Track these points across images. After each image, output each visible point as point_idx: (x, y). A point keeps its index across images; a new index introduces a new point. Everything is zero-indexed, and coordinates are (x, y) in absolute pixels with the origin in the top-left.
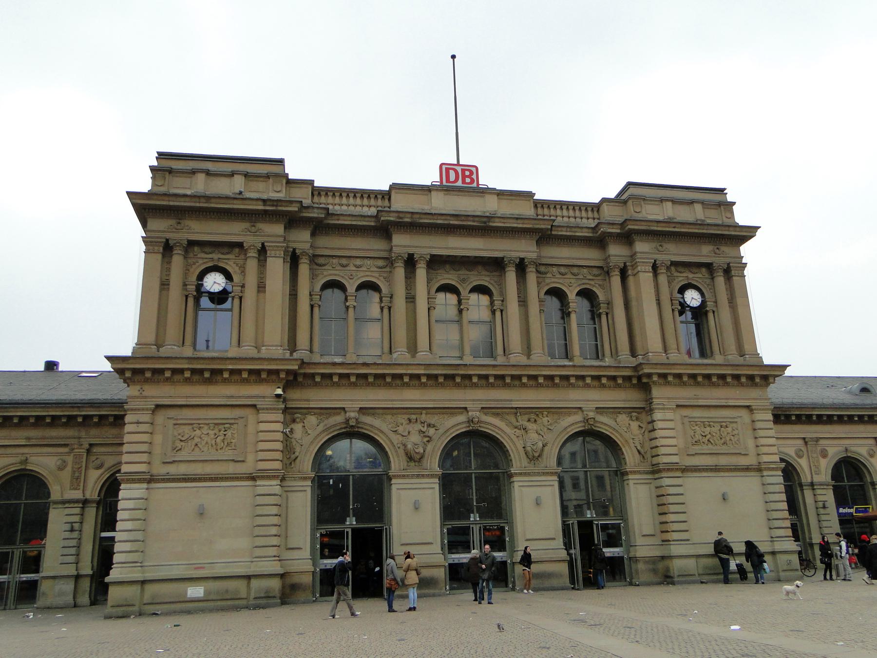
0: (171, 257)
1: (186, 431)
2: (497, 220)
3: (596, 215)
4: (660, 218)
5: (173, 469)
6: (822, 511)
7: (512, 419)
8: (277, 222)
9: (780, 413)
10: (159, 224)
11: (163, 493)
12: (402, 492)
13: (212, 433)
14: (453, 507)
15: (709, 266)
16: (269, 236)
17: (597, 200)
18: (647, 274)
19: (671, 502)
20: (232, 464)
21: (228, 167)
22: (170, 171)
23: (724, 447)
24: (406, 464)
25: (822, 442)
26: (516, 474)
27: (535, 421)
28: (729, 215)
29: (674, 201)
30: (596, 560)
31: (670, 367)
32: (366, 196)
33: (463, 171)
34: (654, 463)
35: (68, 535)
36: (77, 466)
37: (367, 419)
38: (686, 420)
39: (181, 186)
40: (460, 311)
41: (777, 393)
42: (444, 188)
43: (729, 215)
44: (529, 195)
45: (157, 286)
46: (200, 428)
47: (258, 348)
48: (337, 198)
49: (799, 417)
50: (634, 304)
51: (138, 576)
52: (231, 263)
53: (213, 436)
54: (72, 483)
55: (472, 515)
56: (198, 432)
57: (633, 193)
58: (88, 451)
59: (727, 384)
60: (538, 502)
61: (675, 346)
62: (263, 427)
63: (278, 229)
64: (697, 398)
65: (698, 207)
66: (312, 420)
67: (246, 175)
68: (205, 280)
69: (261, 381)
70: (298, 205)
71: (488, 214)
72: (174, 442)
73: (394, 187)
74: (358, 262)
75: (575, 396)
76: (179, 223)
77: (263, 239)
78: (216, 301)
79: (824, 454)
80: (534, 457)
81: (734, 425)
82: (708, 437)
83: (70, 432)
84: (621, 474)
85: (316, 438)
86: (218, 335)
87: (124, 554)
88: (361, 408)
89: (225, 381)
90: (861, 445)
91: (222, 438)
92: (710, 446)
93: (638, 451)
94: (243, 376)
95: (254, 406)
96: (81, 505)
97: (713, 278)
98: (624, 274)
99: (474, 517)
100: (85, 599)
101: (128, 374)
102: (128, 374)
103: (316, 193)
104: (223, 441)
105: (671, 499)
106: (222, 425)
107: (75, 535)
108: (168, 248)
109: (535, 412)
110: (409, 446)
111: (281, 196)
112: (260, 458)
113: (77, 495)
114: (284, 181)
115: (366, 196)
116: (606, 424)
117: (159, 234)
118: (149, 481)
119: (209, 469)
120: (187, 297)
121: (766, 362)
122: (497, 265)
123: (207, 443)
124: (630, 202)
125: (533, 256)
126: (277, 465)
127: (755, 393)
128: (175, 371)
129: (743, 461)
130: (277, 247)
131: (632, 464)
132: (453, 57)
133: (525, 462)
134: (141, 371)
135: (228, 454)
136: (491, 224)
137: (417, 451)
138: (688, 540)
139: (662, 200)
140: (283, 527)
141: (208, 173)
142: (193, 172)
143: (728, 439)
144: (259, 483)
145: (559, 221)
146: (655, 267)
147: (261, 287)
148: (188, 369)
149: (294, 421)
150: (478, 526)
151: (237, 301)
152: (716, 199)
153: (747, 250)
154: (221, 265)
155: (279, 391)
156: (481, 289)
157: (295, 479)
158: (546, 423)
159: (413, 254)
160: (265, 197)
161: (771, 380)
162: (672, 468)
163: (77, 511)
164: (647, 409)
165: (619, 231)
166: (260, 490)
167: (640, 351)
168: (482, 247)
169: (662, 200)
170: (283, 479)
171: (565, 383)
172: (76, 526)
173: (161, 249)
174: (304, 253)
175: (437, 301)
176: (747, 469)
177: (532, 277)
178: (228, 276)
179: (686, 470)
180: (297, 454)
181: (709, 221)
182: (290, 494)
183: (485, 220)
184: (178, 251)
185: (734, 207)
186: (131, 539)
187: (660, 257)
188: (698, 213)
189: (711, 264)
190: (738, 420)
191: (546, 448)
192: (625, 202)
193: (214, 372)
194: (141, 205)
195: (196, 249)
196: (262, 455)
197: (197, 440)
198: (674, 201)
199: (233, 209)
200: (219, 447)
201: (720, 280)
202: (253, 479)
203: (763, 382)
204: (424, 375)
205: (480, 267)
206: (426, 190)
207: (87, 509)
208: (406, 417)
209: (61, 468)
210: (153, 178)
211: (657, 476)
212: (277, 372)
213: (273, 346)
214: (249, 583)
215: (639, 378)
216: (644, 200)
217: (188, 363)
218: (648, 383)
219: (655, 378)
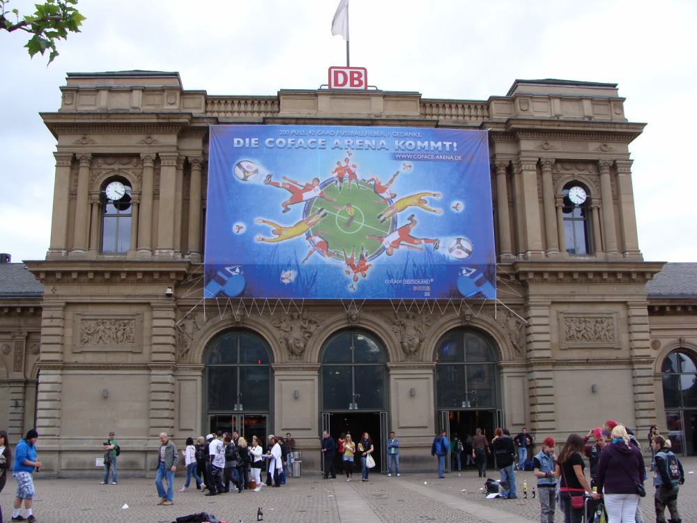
0: (79, 168)
1: (92, 325)
3: (485, 113)
4: (547, 116)
5: (80, 359)
8: (170, 133)
9: (687, 304)
10: (70, 140)
11: (76, 380)
12: (283, 383)
13: (113, 327)
16: (163, 146)
17: (486, 99)
18: (531, 173)
19: (539, 393)
20: (130, 355)
21: (127, 83)
22: (78, 90)
23: (599, 342)
24: (287, 357)
26: (392, 367)
27: (414, 317)
28: (618, 111)
29: (562, 98)
31: (545, 265)
32: (256, 102)
33: (352, 73)
34: (528, 357)
35: (13, 409)
36: (19, 351)
38: (561, 315)
39: (87, 104)
41: (654, 286)
42: (332, 93)
43: (618, 111)
44: (415, 96)
45: (67, 197)
46: (103, 323)
47: (152, 251)
48: (229, 105)
50: (518, 201)
51: (55, 446)
52: (130, 173)
53: (114, 331)
54: (15, 367)
55: (351, 405)
56: (102, 327)
57: (519, 92)
58: (27, 338)
59: (604, 281)
60: (412, 394)
61: (557, 244)
62: (156, 323)
63: (171, 139)
65: (587, 104)
67: (144, 90)
68: (108, 189)
69: (154, 282)
70: (189, 117)
71: (373, 117)
72: (82, 335)
73: (283, 93)
76: (84, 138)
77: (157, 150)
78: (118, 206)
80: (409, 352)
81: (610, 320)
82: (582, 333)
83: (12, 321)
84: (497, 369)
85: (205, 332)
86: (119, 239)
87: (44, 429)
89: (123, 281)
91: (122, 332)
92: (584, 340)
93: (515, 346)
94: (171, 277)
95: (149, 304)
96: (23, 385)
97: (599, 175)
98: (509, 170)
99: (239, 408)
101: (42, 276)
102: (42, 276)
103: (209, 102)
104: (123, 335)
105: (540, 391)
106: (123, 321)
107: (19, 410)
108: (75, 161)
110: (291, 341)
111: (174, 108)
112: (154, 350)
113: (19, 376)
114: (178, 94)
115: (256, 102)
117: (534, 154)
118: (63, 368)
119: (103, 359)
120: (92, 205)
121: (646, 259)
123: (109, 336)
124: (517, 100)
128: (80, 273)
130: (170, 156)
131: (507, 358)
133: (402, 356)
134: (53, 273)
135: (127, 346)
137: (297, 345)
138: (553, 429)
140: (176, 410)
141: (110, 90)
142: (97, 90)
143: (602, 334)
144: (153, 372)
146: (539, 165)
147: (156, 195)
148: (91, 271)
150: (240, 416)
151: (135, 208)
152: (608, 96)
153: (634, 147)
154: (121, 175)
155: (169, 291)
157: (186, 369)
160: (158, 110)
161: (648, 276)
163: (20, 389)
164: (524, 306)
165: (503, 130)
166: (154, 379)
167: (521, 250)
170: (175, 369)
171: (612, 279)
172: (20, 402)
173: (70, 163)
174: (196, 160)
176: (616, 362)
178: (125, 182)
180: (188, 347)
182: (182, 382)
184: (84, 164)
185: (625, 103)
186: (49, 416)
187: (544, 155)
188: (588, 109)
189: (598, 161)
190: (614, 316)
191: (423, 344)
192: (513, 100)
193: (114, 274)
194: (52, 123)
195: (100, 161)
196: (155, 348)
197: (101, 334)
198: (562, 98)
199: (131, 123)
200: (119, 340)
201: (606, 178)
202: (149, 368)
203: (640, 278)
204: (635, 272)
206: (313, 94)
207: (28, 389)
209: (6, 353)
210: (64, 97)
211: (530, 369)
212: (168, 273)
213: (167, 251)
214: (146, 457)
215: (517, 276)
216: (531, 98)
217: (91, 266)
218: (525, 280)
219: (531, 276)
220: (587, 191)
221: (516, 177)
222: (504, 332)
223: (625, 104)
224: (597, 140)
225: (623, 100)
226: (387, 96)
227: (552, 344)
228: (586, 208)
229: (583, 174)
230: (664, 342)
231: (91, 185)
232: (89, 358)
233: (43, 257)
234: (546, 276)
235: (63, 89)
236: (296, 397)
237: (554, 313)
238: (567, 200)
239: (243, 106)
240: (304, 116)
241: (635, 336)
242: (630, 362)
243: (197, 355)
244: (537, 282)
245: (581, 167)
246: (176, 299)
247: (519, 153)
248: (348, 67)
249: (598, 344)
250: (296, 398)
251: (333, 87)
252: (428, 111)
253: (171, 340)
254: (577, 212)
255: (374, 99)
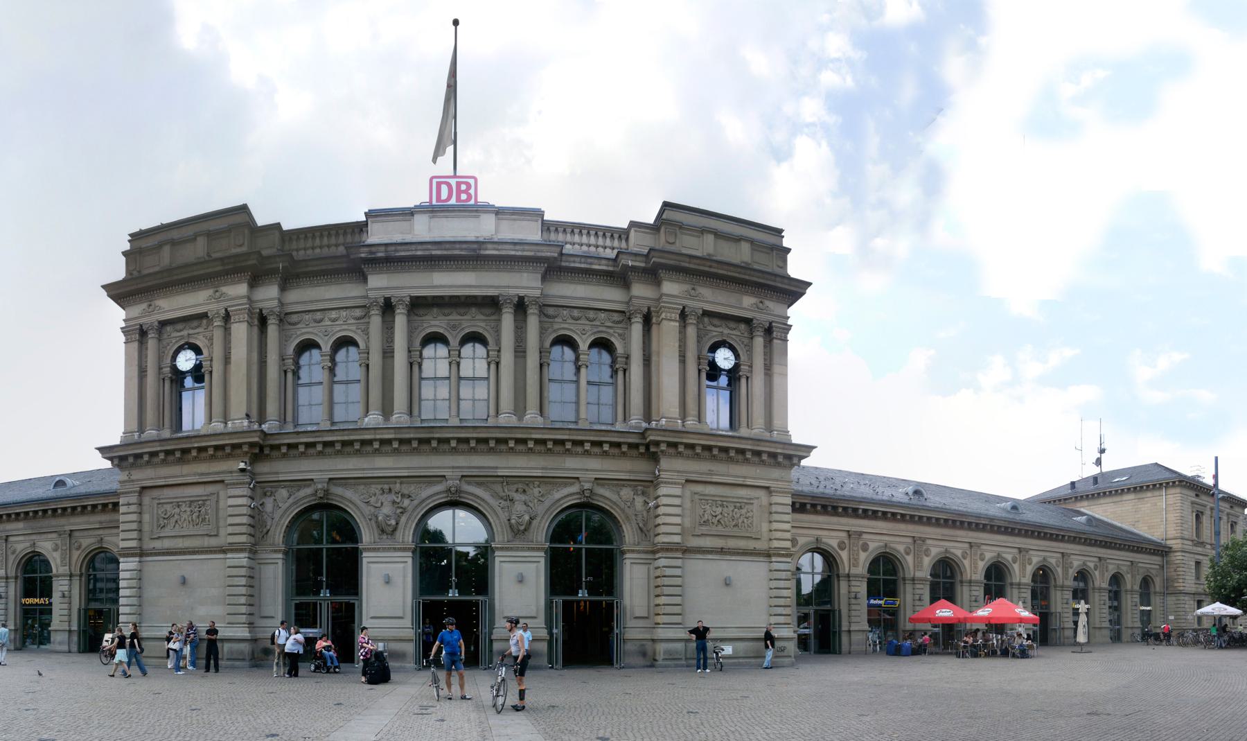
2: (489, 246)
5: (158, 544)
6: (853, 601)
7: (498, 488)
8: (239, 282)
10: (137, 310)
14: (561, 575)
15: (748, 321)
18: (673, 323)
20: (206, 538)
25: (865, 536)
28: (781, 264)
29: (718, 235)
30: (587, 635)
33: (459, 184)
37: (337, 490)
38: (697, 497)
39: (152, 265)
40: (578, 369)
43: (781, 264)
44: (537, 214)
49: (845, 509)
50: (654, 358)
56: (177, 510)
61: (696, 413)
64: (711, 473)
65: (745, 246)
66: (283, 493)
74: (334, 314)
75: (572, 464)
79: (865, 548)
81: (750, 507)
88: (330, 479)
90: (832, 537)
93: (641, 529)
95: (222, 481)
98: (647, 320)
99: (325, 593)
100: (75, 648)
108: (143, 333)
109: (527, 480)
116: (607, 497)
121: (795, 440)
122: (491, 304)
125: (537, 293)
126: (243, 539)
127: (776, 473)
129: (751, 545)
132: (456, 23)
136: (483, 252)
139: (703, 231)
141: (174, 243)
142: (160, 246)
145: (568, 249)
146: (683, 315)
147: (227, 360)
149: (265, 494)
152: (769, 241)
154: (192, 341)
155: (242, 465)
156: (602, 344)
158: (537, 494)
159: (389, 299)
161: (795, 460)
162: (669, 548)
164: (649, 485)
165: (643, 265)
166: (229, 562)
168: (474, 283)
169: (703, 231)
171: (756, 459)
174: (272, 312)
175: (428, 369)
177: (533, 322)
178: (197, 350)
179: (687, 551)
181: (756, 267)
183: (475, 246)
188: (741, 254)
189: (751, 320)
190: (755, 501)
191: (535, 522)
195: (169, 328)
196: (230, 530)
197: (176, 517)
198: (718, 235)
201: (759, 342)
203: (786, 462)
205: (473, 310)
206: (408, 214)
208: (379, 487)
212: (239, 446)
215: (647, 446)
216: (681, 228)
219: (663, 447)
220: (737, 356)
221: (654, 328)
222: (630, 512)
223: (789, 256)
224: (753, 294)
225: (788, 250)
226: (499, 212)
227: (683, 529)
228: (733, 374)
229: (734, 334)
230: (802, 541)
231: (160, 358)
232: (167, 544)
233: (117, 442)
234: (681, 448)
235: (125, 254)
236: (388, 581)
237: (688, 494)
238: (713, 365)
239: (325, 239)
240: (394, 241)
241: (775, 526)
242: (768, 554)
243: (278, 536)
244: (671, 456)
245: (732, 325)
246: (253, 475)
247: (658, 300)
248: (455, 176)
249: (736, 532)
250: (387, 583)
251: (434, 202)
252: (553, 236)
253: (245, 520)
254: (723, 380)
255: (484, 217)
